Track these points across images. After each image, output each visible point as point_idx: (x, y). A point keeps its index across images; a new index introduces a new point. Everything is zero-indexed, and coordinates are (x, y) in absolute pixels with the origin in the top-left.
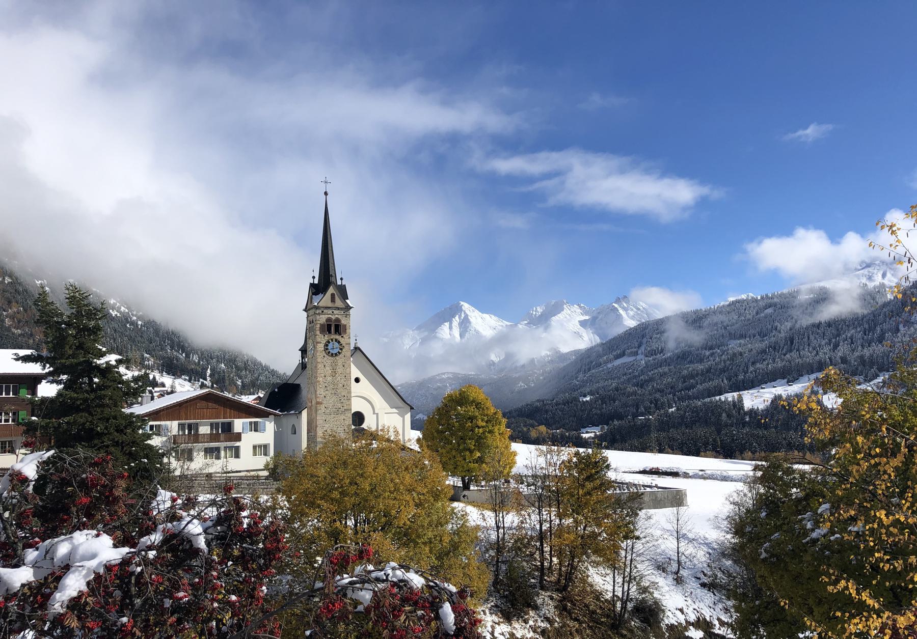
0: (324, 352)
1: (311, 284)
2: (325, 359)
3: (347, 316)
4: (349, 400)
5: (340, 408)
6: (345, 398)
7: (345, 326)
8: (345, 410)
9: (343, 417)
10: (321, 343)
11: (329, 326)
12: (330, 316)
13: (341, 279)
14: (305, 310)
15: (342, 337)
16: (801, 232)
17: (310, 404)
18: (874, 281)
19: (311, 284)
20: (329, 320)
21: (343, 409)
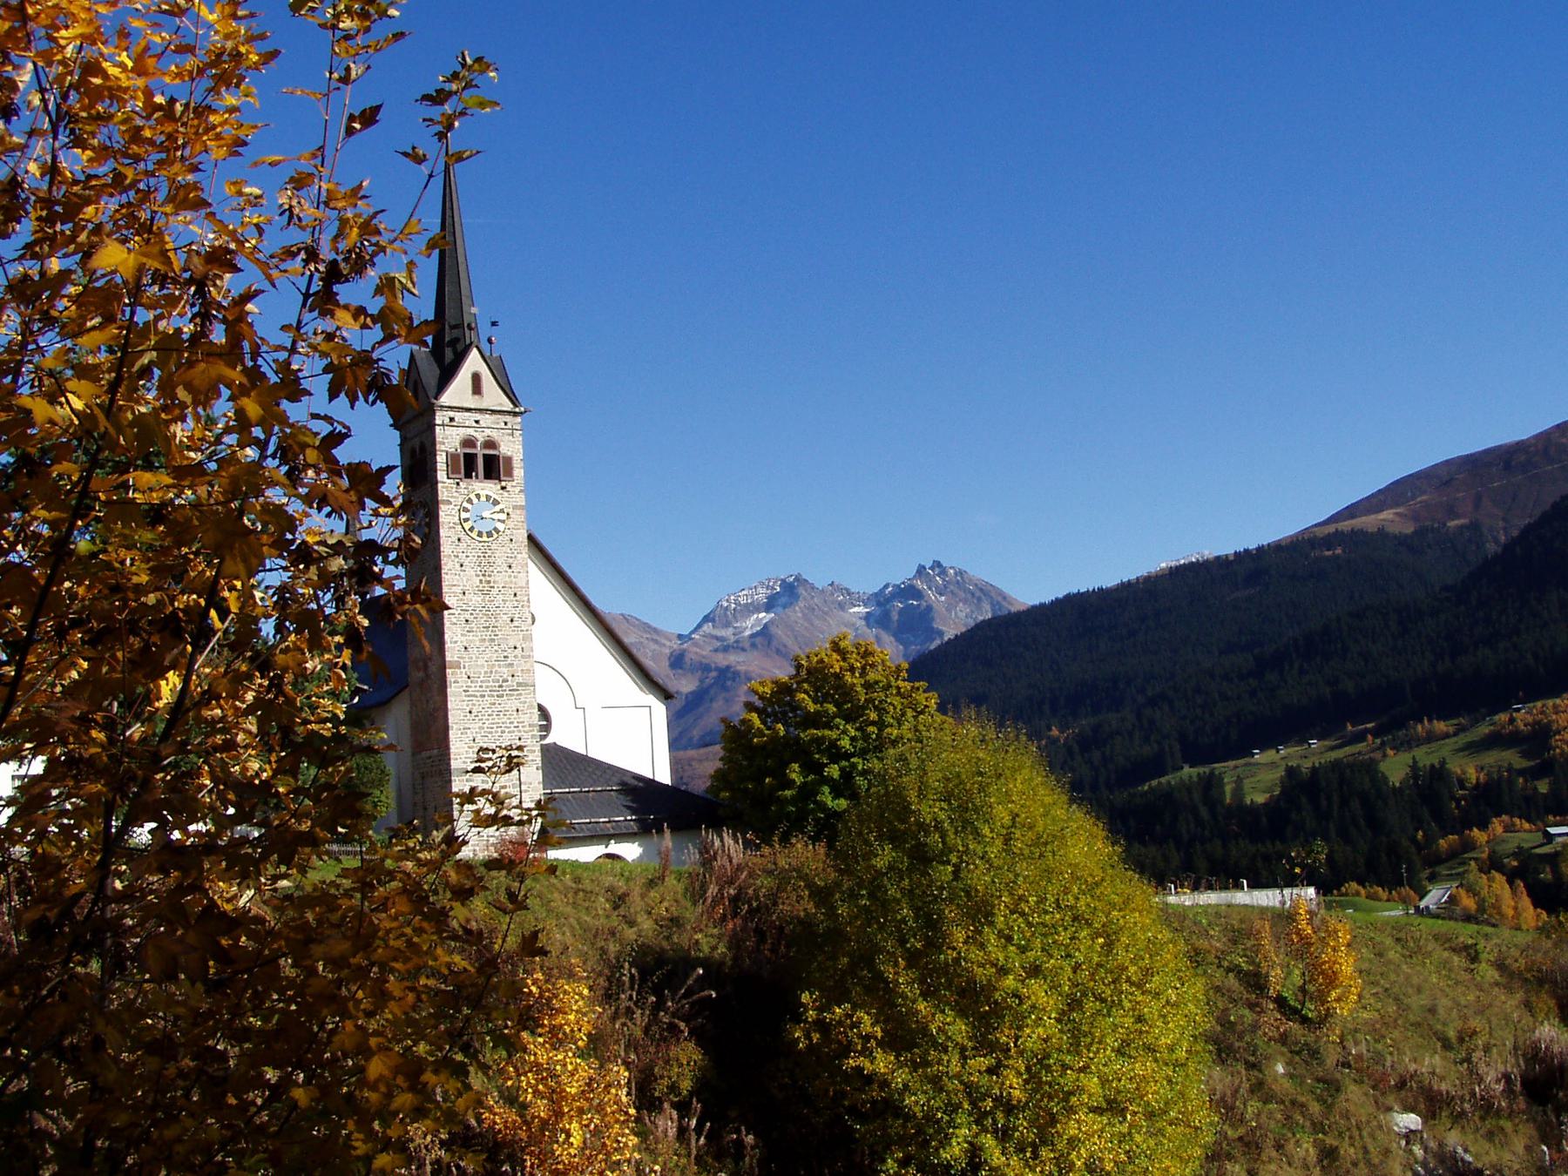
2: (463, 545)
8: (519, 684)
12: (471, 431)
15: (503, 488)
20: (469, 442)
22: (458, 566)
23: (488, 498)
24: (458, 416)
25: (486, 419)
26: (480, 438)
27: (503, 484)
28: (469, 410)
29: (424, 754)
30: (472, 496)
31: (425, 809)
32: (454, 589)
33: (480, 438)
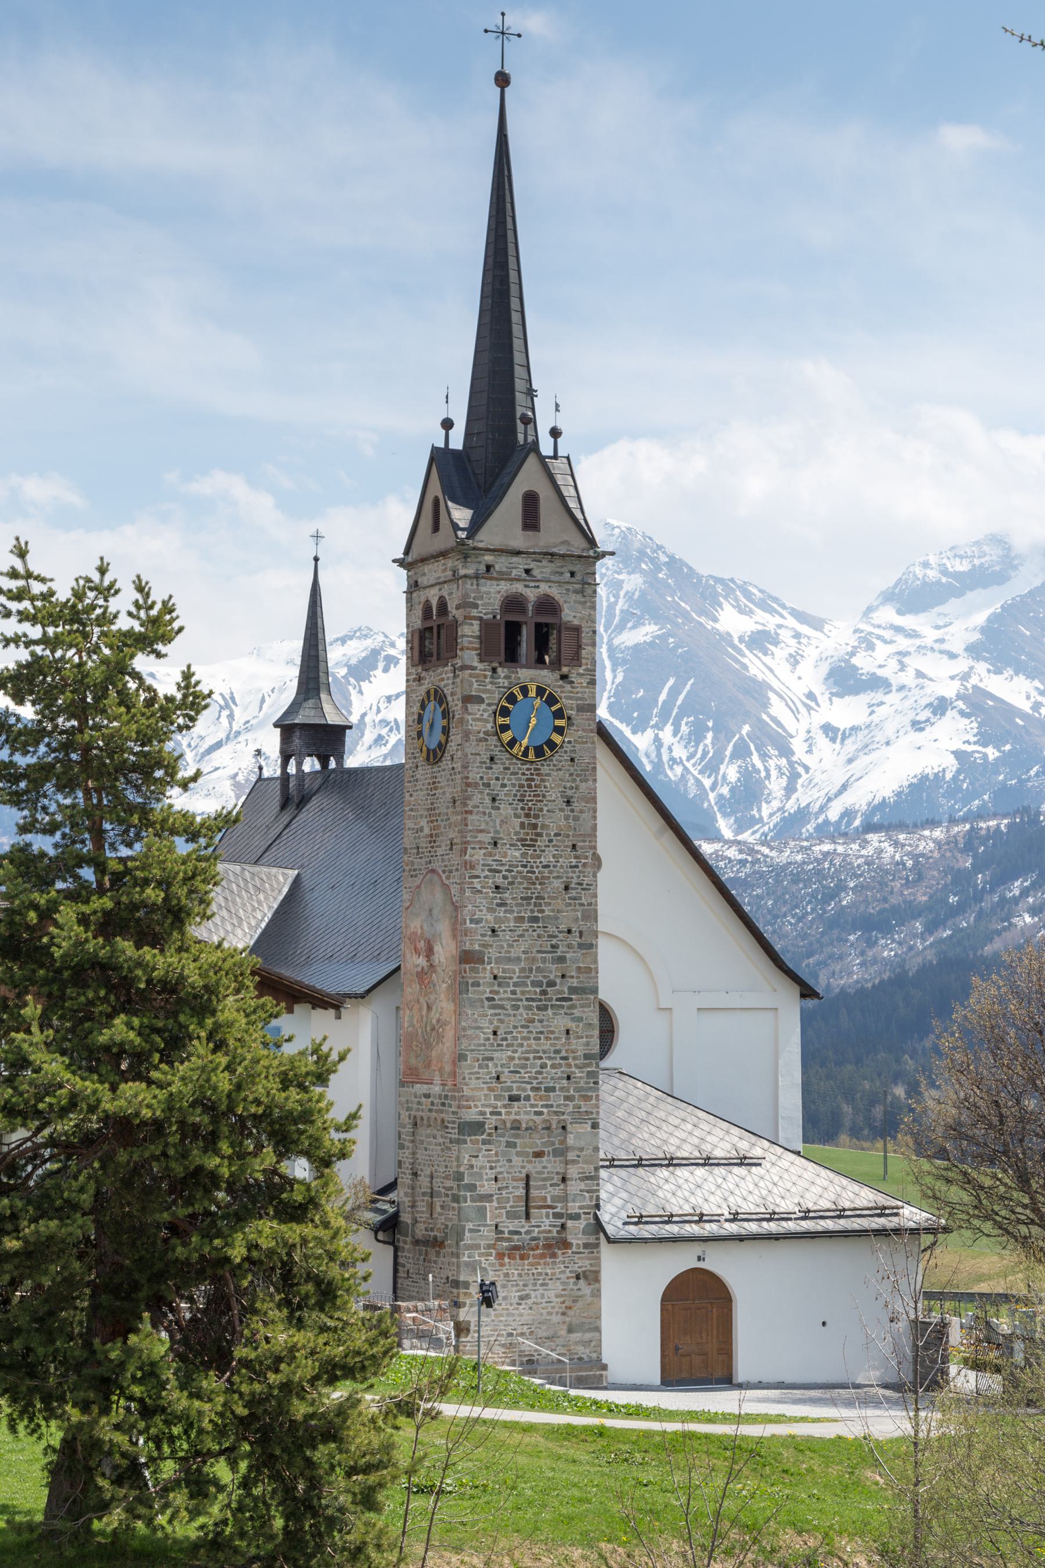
0: (493, 740)
1: (435, 450)
2: (498, 768)
3: (587, 587)
4: (589, 948)
5: (551, 984)
6: (575, 940)
7: (577, 630)
8: (573, 990)
9: (560, 1022)
10: (480, 700)
11: (513, 630)
12: (518, 588)
13: (555, 433)
14: (401, 563)
15: (564, 677)
16: (847, 697)
17: (422, 961)
18: (277, 1534)
19: (435, 450)
20: (513, 604)
21: (563, 988)
22: (488, 801)
23: (540, 691)
24: (501, 564)
25: (542, 569)
26: (531, 595)
27: (565, 670)
28: (518, 553)
29: (420, 1089)
30: (516, 691)
31: (415, 1174)
32: (481, 837)
33: (531, 595)
